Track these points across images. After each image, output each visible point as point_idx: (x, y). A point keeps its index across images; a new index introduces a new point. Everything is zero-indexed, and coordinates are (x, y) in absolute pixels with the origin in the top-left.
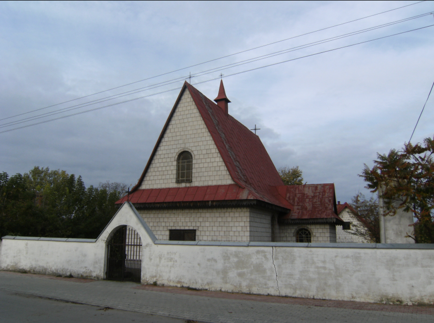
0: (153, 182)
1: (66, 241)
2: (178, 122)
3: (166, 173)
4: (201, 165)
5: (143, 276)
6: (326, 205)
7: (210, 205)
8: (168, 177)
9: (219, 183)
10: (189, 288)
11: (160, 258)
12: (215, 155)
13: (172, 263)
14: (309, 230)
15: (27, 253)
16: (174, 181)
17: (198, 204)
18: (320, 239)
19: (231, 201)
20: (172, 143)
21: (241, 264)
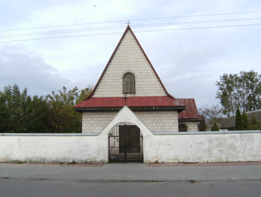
0: (104, 93)
1: (66, 136)
2: (122, 52)
3: (114, 86)
4: (142, 83)
5: (146, 158)
6: (193, 111)
7: (154, 109)
8: (116, 89)
9: (156, 95)
10: (184, 163)
11: (160, 144)
12: (152, 77)
13: (170, 147)
14: (186, 125)
15: (20, 147)
16: (122, 92)
17: (145, 108)
18: (193, 130)
19: (169, 106)
20: (119, 66)
21: (220, 145)
